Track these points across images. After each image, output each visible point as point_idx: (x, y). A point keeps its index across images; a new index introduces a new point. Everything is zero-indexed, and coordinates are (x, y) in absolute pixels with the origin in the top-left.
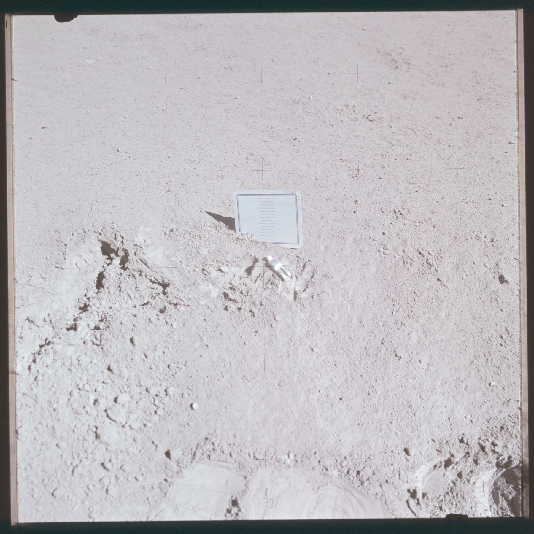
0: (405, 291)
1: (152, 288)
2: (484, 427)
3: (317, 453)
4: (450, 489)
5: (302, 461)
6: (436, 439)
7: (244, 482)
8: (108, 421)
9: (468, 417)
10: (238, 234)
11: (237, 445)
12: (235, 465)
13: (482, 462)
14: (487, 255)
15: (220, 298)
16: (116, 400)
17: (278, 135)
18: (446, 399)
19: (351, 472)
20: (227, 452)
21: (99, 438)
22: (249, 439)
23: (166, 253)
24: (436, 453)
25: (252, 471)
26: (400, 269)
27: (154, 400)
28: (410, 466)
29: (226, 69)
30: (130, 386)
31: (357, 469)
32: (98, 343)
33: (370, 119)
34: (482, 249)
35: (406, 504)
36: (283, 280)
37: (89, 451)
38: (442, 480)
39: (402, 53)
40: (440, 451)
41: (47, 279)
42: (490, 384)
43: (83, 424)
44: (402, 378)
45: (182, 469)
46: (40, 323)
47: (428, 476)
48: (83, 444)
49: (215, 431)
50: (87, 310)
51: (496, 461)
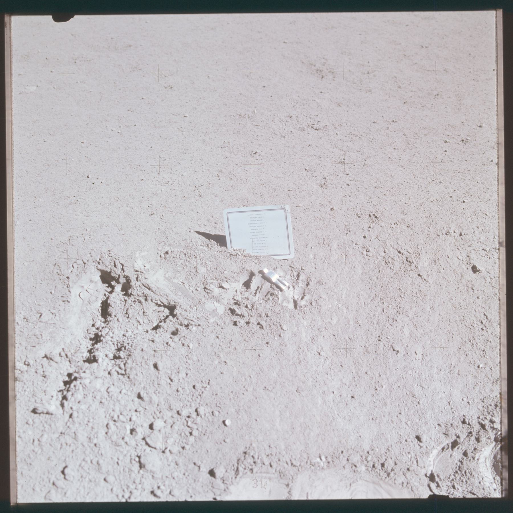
0: (391, 288)
1: (159, 312)
2: (480, 407)
3: (344, 452)
4: (458, 468)
5: (333, 461)
6: (441, 424)
7: (287, 490)
8: (148, 449)
9: (465, 399)
10: (230, 249)
12: (276, 475)
13: (483, 439)
15: (227, 315)
16: (151, 427)
19: (376, 465)
20: (267, 463)
21: (144, 467)
22: (283, 447)
23: (167, 276)
25: (293, 478)
26: (383, 269)
27: (187, 422)
28: (424, 452)
29: (166, 88)
30: (162, 411)
32: (123, 372)
35: (428, 488)
36: (281, 290)
38: (450, 461)
39: (325, 63)
40: (447, 435)
41: (57, 314)
42: (479, 367)
43: (125, 455)
45: (228, 486)
46: (57, 359)
47: (437, 458)
48: (130, 475)
49: (251, 444)
50: (101, 341)
51: (494, 436)
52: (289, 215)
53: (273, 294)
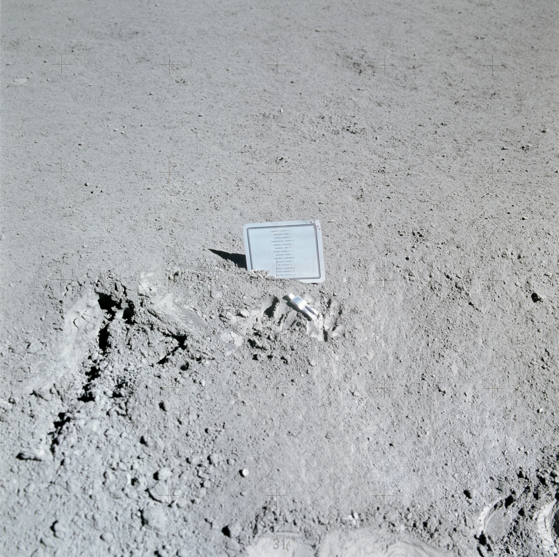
0: (437, 319)
1: (166, 343)
2: (540, 458)
3: (381, 509)
4: (513, 528)
5: (367, 519)
6: (494, 477)
8: (152, 502)
9: (522, 449)
10: (250, 271)
11: (299, 511)
13: (543, 495)
14: (516, 273)
15: (246, 347)
17: (260, 155)
18: (497, 433)
19: (417, 524)
20: (290, 520)
21: (147, 523)
22: (309, 502)
24: (497, 491)
25: (320, 538)
26: (428, 296)
27: (198, 471)
28: (473, 509)
29: (178, 82)
30: (169, 458)
31: (423, 521)
33: (351, 130)
34: (510, 267)
35: (477, 552)
36: (309, 319)
37: (139, 539)
38: (503, 520)
39: (364, 55)
41: (48, 344)
42: (538, 411)
43: (125, 509)
44: (448, 414)
45: (245, 546)
46: (48, 396)
47: (488, 517)
49: (272, 498)
51: (555, 492)
52: (320, 233)
53: (300, 324)
